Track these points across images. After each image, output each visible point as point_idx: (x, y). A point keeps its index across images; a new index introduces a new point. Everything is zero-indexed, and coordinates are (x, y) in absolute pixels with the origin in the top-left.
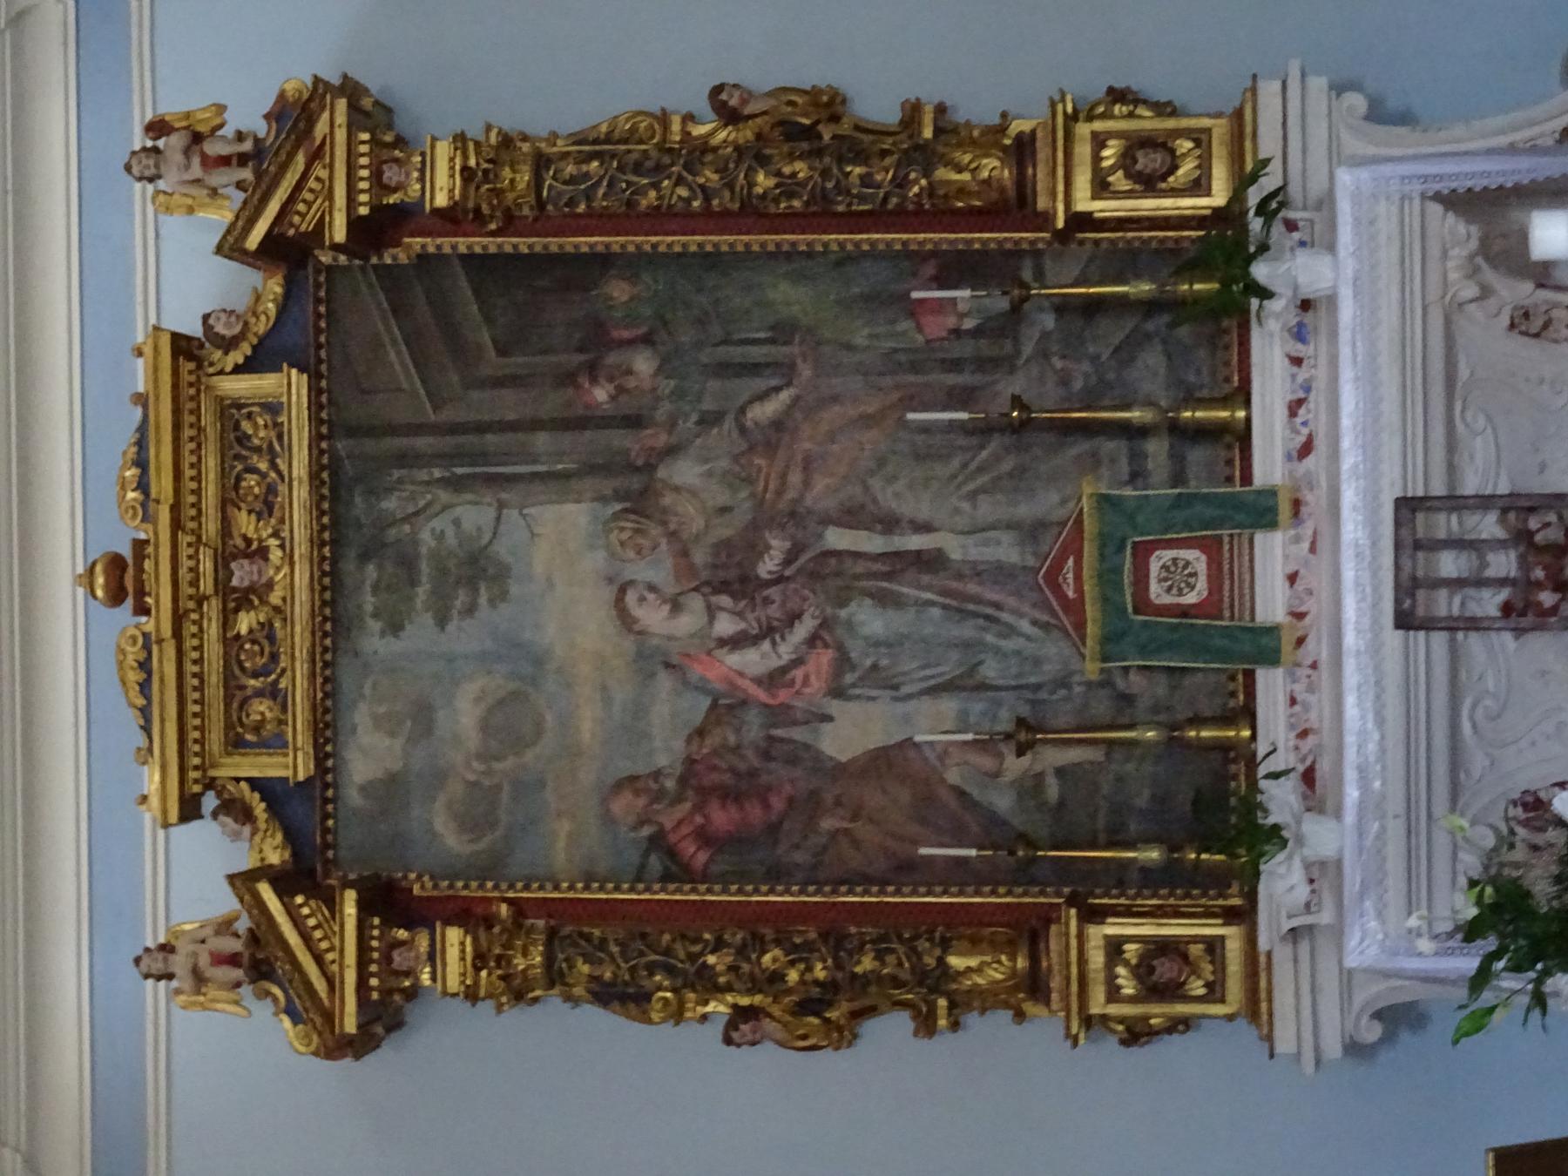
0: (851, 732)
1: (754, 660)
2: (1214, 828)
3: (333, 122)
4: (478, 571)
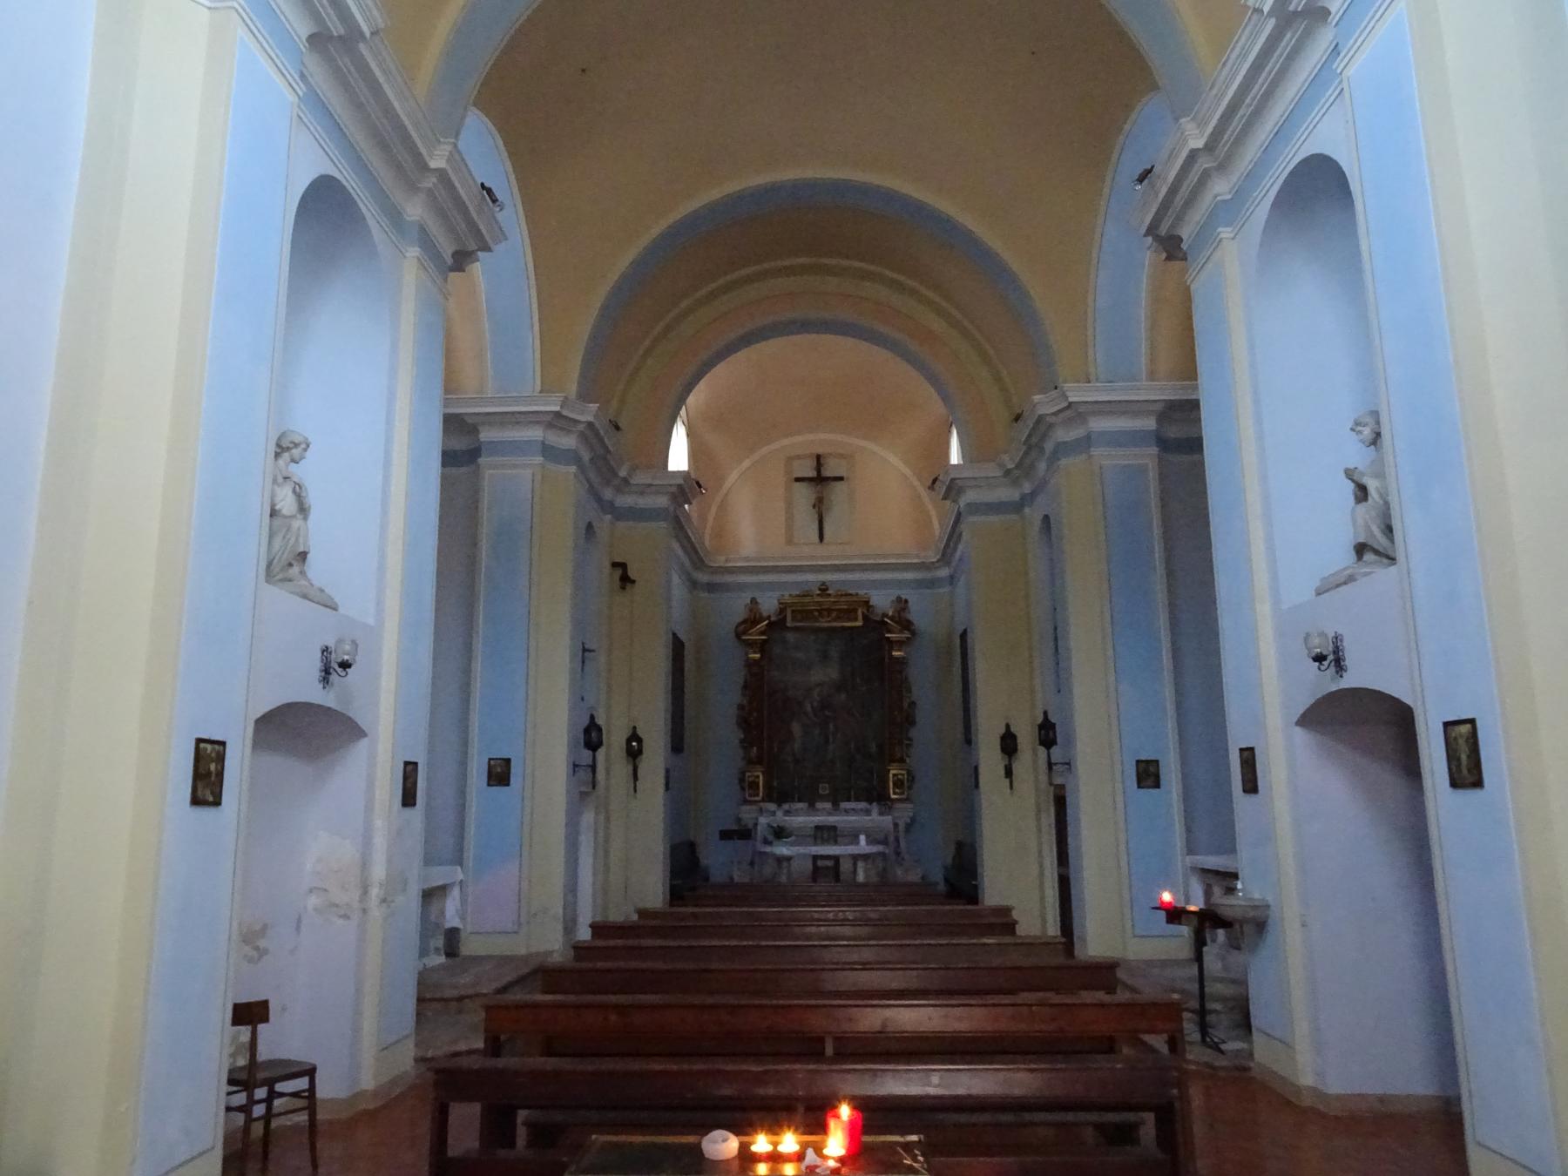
0: (796, 728)
1: (809, 709)
2: (780, 795)
3: (907, 634)
4: (825, 657)
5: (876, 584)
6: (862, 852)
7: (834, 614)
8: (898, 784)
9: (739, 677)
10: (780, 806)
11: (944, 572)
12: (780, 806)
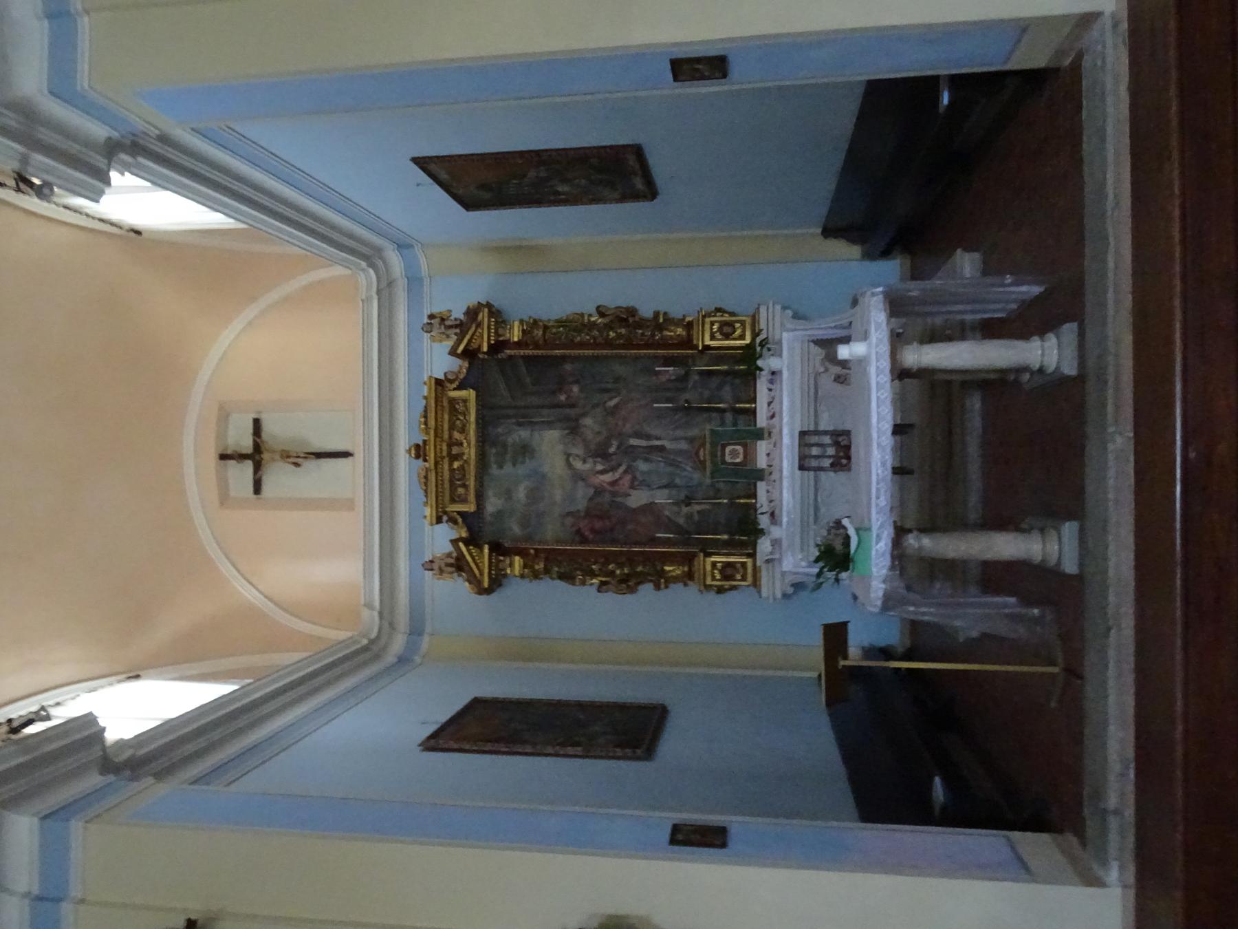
0: (637, 499)
1: (608, 478)
2: (744, 529)
4: (525, 450)
5: (414, 364)
6: (885, 348)
7: (456, 435)
8: (727, 330)
9: (552, 590)
10: (762, 532)
11: (394, 259)
12: (762, 532)
